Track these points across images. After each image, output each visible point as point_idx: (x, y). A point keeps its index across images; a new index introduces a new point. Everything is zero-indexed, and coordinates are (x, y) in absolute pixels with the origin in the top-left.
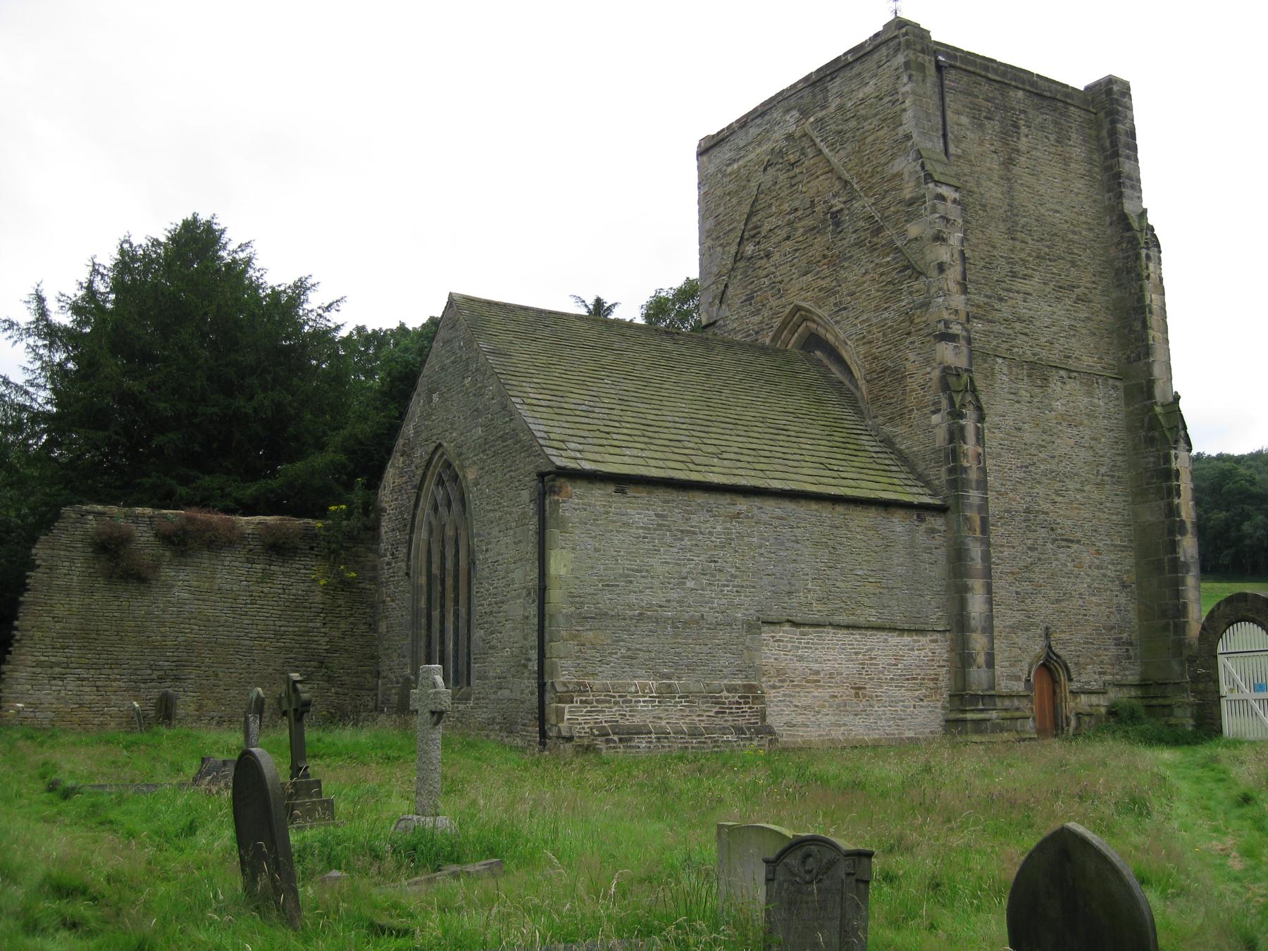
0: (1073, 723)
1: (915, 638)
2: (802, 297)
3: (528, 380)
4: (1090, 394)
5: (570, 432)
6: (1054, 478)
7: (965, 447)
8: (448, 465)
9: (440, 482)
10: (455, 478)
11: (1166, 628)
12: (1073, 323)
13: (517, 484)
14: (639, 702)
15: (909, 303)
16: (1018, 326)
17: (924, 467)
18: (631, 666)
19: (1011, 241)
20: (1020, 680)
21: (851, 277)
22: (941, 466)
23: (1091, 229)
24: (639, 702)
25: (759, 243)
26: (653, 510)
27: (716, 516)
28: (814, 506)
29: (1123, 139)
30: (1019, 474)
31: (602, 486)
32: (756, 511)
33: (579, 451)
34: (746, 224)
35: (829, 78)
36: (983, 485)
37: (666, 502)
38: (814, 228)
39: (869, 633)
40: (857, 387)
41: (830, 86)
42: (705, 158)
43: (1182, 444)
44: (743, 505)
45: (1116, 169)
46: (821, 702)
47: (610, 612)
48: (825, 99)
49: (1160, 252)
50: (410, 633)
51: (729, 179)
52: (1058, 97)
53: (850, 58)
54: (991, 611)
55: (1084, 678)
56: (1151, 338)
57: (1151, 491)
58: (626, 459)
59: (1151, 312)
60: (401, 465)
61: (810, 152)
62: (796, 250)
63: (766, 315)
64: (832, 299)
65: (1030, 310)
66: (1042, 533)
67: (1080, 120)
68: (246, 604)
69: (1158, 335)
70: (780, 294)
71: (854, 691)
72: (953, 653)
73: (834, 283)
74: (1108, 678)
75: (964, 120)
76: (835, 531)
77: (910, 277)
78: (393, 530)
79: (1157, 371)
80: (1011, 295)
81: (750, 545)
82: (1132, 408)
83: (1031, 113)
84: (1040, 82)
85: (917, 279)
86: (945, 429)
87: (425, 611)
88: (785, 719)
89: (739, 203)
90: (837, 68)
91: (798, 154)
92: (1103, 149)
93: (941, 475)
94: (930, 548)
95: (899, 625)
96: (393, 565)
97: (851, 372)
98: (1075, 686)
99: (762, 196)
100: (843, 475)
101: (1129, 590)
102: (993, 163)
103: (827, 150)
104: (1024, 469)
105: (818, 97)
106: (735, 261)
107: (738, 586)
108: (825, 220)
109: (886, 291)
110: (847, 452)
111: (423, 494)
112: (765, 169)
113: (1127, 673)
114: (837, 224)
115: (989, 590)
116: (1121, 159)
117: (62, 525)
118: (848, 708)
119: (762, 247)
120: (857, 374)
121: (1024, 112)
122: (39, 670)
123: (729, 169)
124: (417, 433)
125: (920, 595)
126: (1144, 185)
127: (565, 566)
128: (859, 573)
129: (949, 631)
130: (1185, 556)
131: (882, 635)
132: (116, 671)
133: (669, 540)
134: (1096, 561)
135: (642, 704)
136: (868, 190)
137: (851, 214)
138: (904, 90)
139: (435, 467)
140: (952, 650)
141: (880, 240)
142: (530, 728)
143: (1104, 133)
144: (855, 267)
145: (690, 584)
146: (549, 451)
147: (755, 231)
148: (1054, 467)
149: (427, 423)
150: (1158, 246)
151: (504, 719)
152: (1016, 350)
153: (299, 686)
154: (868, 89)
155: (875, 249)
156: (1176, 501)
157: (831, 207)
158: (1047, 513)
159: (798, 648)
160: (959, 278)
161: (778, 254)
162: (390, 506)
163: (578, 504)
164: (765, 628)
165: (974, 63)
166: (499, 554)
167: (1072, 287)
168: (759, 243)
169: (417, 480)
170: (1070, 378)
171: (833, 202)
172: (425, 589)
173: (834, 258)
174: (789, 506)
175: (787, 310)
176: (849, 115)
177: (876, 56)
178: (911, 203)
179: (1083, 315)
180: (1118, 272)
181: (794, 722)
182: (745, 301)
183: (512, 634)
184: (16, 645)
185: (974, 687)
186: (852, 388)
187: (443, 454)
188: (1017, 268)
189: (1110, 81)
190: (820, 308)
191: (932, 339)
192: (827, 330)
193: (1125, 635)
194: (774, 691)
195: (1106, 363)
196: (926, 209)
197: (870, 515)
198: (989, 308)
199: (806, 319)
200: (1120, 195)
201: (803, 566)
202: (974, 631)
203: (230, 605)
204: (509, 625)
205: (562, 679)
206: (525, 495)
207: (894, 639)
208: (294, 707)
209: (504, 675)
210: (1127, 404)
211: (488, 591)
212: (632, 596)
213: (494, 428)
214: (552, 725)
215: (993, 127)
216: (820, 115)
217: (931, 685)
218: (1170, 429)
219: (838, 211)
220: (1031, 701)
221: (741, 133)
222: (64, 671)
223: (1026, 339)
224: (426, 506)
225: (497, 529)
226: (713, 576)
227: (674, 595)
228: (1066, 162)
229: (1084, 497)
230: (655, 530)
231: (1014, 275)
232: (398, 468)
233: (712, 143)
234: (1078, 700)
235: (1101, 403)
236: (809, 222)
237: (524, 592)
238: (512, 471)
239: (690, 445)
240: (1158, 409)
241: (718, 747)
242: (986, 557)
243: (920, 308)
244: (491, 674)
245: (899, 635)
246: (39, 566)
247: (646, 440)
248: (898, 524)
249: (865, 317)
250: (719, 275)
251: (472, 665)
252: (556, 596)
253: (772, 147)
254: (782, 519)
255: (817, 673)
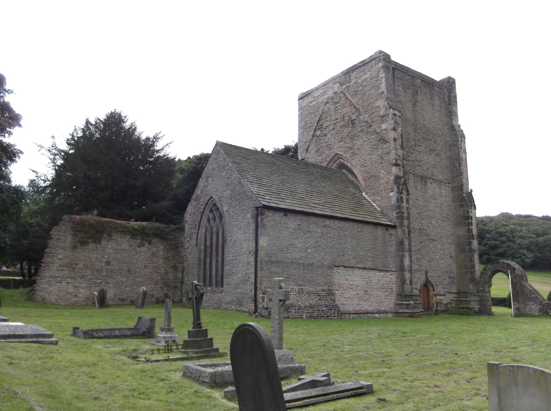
0: (435, 306)
1: (385, 273)
2: (339, 150)
3: (248, 173)
4: (440, 188)
5: (266, 193)
6: (428, 218)
7: (403, 204)
8: (215, 205)
9: (211, 211)
10: (218, 209)
11: (467, 273)
12: (435, 163)
13: (245, 211)
14: (291, 295)
15: (381, 152)
16: (417, 163)
17: (387, 211)
18: (288, 281)
19: (415, 133)
20: (418, 290)
21: (358, 143)
22: (394, 211)
23: (441, 130)
24: (291, 295)
25: (322, 131)
26: (297, 223)
27: (318, 226)
28: (352, 224)
29: (453, 99)
30: (417, 216)
31: (279, 213)
32: (332, 224)
33: (286, 195)
34: (317, 124)
35: (352, 72)
36: (408, 218)
37: (301, 220)
38: (344, 126)
39: (369, 271)
40: (359, 182)
41: (352, 74)
42: (301, 101)
43: (473, 207)
44: (328, 222)
45: (450, 109)
46: (353, 296)
47: (281, 260)
48: (350, 79)
49: (465, 139)
50: (197, 267)
51: (310, 108)
52: (431, 83)
53: (360, 65)
54: (411, 264)
55: (438, 290)
56: (462, 169)
57: (462, 223)
58: (287, 204)
59: (462, 160)
60: (194, 205)
61: (343, 98)
62: (337, 133)
63: (324, 156)
64: (351, 151)
65: (421, 157)
66: (425, 237)
67: (438, 91)
68: (134, 255)
69: (464, 168)
70: (330, 149)
71: (364, 292)
72: (398, 280)
73: (352, 145)
74: (446, 290)
75: (400, 89)
76: (358, 233)
77: (382, 143)
78: (190, 229)
79: (464, 181)
80: (415, 152)
81: (330, 237)
82: (454, 194)
83: (422, 88)
84: (425, 77)
85: (385, 144)
86: (396, 198)
87: (203, 259)
88: (341, 302)
89: (315, 116)
90: (355, 68)
91: (338, 99)
92: (446, 102)
93: (394, 214)
94: (390, 241)
95: (380, 268)
96: (190, 242)
97: (356, 177)
98: (435, 292)
99: (324, 114)
100: (360, 213)
101: (453, 259)
102: (409, 105)
103: (350, 98)
104: (419, 214)
105: (347, 79)
106: (312, 138)
107: (325, 252)
108: (349, 123)
109: (373, 148)
110: (359, 205)
111: (204, 215)
112: (325, 104)
113: (452, 288)
114: (354, 124)
115: (411, 256)
116: (452, 106)
117: (63, 222)
118: (363, 299)
119: (323, 132)
120: (359, 177)
121: (420, 87)
122: (51, 279)
123: (311, 105)
124: (202, 193)
125: (386, 258)
126: (459, 116)
127: (265, 242)
128: (367, 249)
129: (396, 271)
130: (474, 247)
131: (374, 272)
132: (83, 280)
133: (302, 234)
134: (442, 248)
135: (292, 295)
136: (365, 112)
137: (359, 121)
138: (382, 76)
139: (209, 205)
140: (397, 278)
141: (371, 130)
142: (250, 304)
143: (446, 97)
144: (360, 140)
145: (309, 251)
146: (260, 199)
147: (321, 127)
148: (429, 214)
149: (206, 189)
150: (464, 137)
151: (238, 300)
152: (416, 171)
153: (198, 287)
154: (366, 76)
155: (368, 133)
156: (471, 227)
157: (351, 118)
158: (426, 230)
159: (346, 276)
160: (400, 144)
161: (330, 135)
162: (189, 220)
163: (271, 219)
164: (335, 268)
165: (404, 69)
166: (237, 238)
167: (434, 150)
168: (322, 131)
169: (202, 210)
170: (434, 182)
171: (352, 116)
172: (203, 251)
173: (352, 136)
174: (343, 223)
175: (333, 155)
176: (359, 85)
177: (370, 64)
178: (383, 116)
179: (438, 160)
180: (450, 146)
181: (344, 303)
182: (316, 151)
183: (242, 268)
184: (42, 269)
185: (406, 292)
186: (357, 183)
187: (213, 200)
188: (417, 143)
189: (450, 78)
190: (346, 154)
191: (391, 165)
192: (348, 162)
193: (452, 275)
194: (337, 291)
195: (445, 178)
196: (389, 118)
197: (370, 228)
198: (408, 156)
199: (339, 158)
200: (452, 119)
201: (347, 245)
202: (406, 271)
203: (128, 255)
204: (240, 265)
205: (264, 286)
206: (249, 216)
207: (378, 273)
208: (195, 296)
209: (238, 283)
210: (453, 192)
211: (232, 251)
212: (289, 255)
213: (236, 190)
214: (260, 303)
215: (409, 92)
216: (348, 85)
217: (390, 291)
218: (469, 202)
219: (354, 120)
220: (421, 298)
221: (316, 92)
222: (61, 279)
223: (419, 167)
224: (204, 220)
225: (236, 228)
226: (317, 248)
227: (303, 255)
228: (433, 106)
229: (438, 225)
230: (297, 230)
231: (416, 145)
232: (193, 205)
233: (304, 95)
234: (436, 297)
235: (444, 192)
236: (342, 123)
237: (248, 252)
238: (243, 206)
239: (307, 200)
240: (464, 195)
241: (320, 312)
242: (410, 244)
243: (386, 154)
244: (233, 283)
245: (380, 272)
246: (53, 238)
247: (292, 197)
248: (379, 231)
249: (364, 157)
250: (306, 142)
251: (224, 280)
252: (261, 253)
253: (328, 97)
254: (341, 228)
255: (352, 285)
